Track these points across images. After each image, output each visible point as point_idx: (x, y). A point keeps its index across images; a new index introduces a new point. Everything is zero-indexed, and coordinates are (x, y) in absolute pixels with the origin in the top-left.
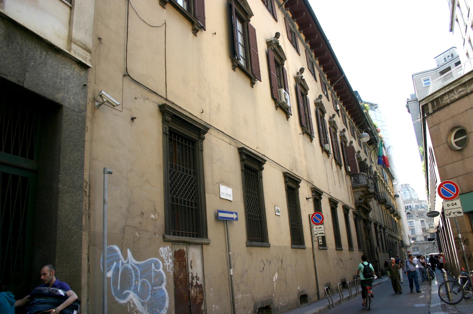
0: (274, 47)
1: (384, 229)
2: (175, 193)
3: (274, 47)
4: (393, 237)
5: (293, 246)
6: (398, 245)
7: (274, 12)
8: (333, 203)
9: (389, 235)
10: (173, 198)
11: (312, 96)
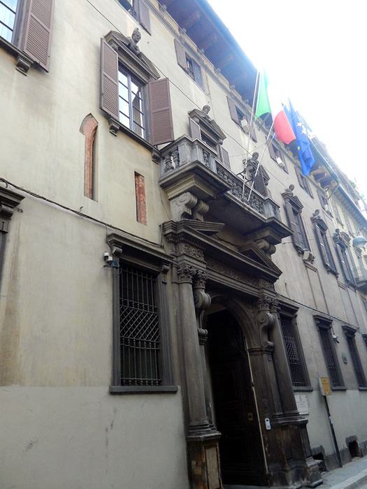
5: (119, 388)
8: (349, 333)
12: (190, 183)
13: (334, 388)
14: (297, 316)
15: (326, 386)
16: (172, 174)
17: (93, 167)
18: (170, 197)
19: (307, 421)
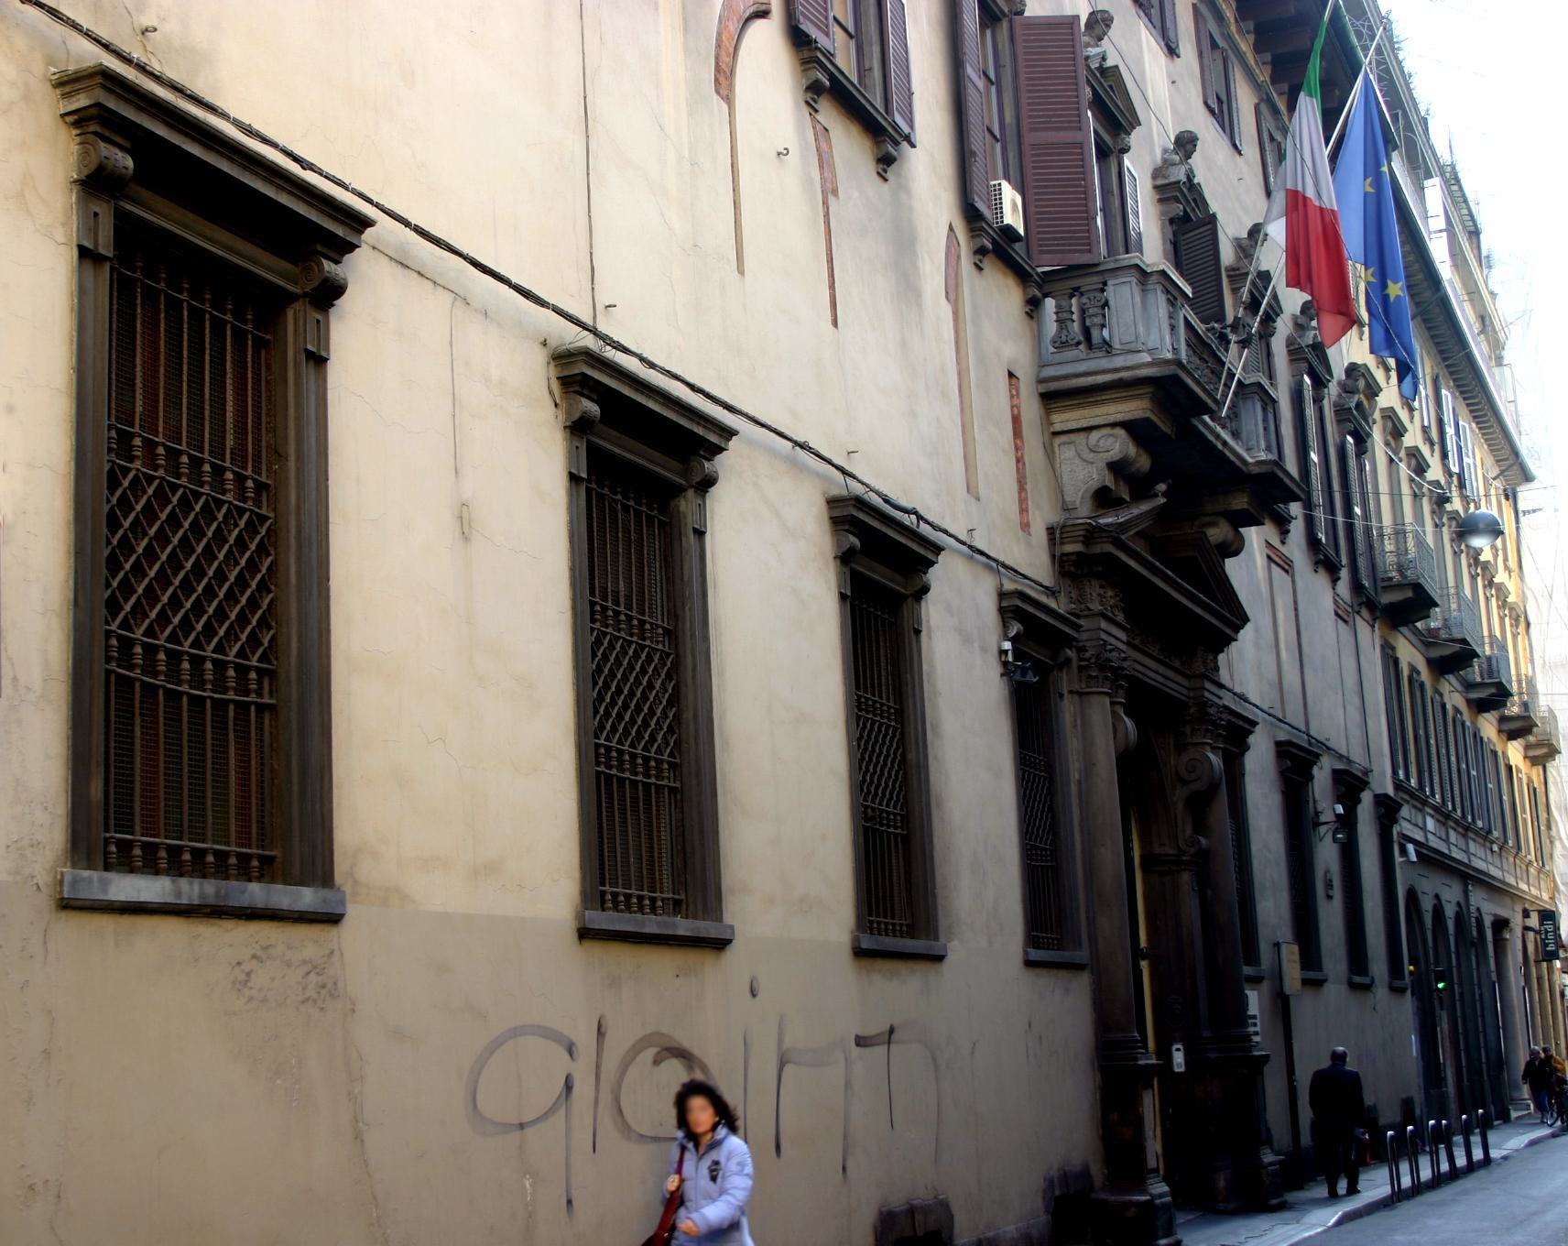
1: (1387, 811)
4: (1468, 877)
5: (1036, 954)
6: (1514, 938)
7: (1169, 24)
8: (1349, 784)
9: (1432, 860)
10: (126, 644)
12: (1134, 408)
14: (925, 589)
15: (1293, 972)
16: (1081, 366)
18: (1058, 427)
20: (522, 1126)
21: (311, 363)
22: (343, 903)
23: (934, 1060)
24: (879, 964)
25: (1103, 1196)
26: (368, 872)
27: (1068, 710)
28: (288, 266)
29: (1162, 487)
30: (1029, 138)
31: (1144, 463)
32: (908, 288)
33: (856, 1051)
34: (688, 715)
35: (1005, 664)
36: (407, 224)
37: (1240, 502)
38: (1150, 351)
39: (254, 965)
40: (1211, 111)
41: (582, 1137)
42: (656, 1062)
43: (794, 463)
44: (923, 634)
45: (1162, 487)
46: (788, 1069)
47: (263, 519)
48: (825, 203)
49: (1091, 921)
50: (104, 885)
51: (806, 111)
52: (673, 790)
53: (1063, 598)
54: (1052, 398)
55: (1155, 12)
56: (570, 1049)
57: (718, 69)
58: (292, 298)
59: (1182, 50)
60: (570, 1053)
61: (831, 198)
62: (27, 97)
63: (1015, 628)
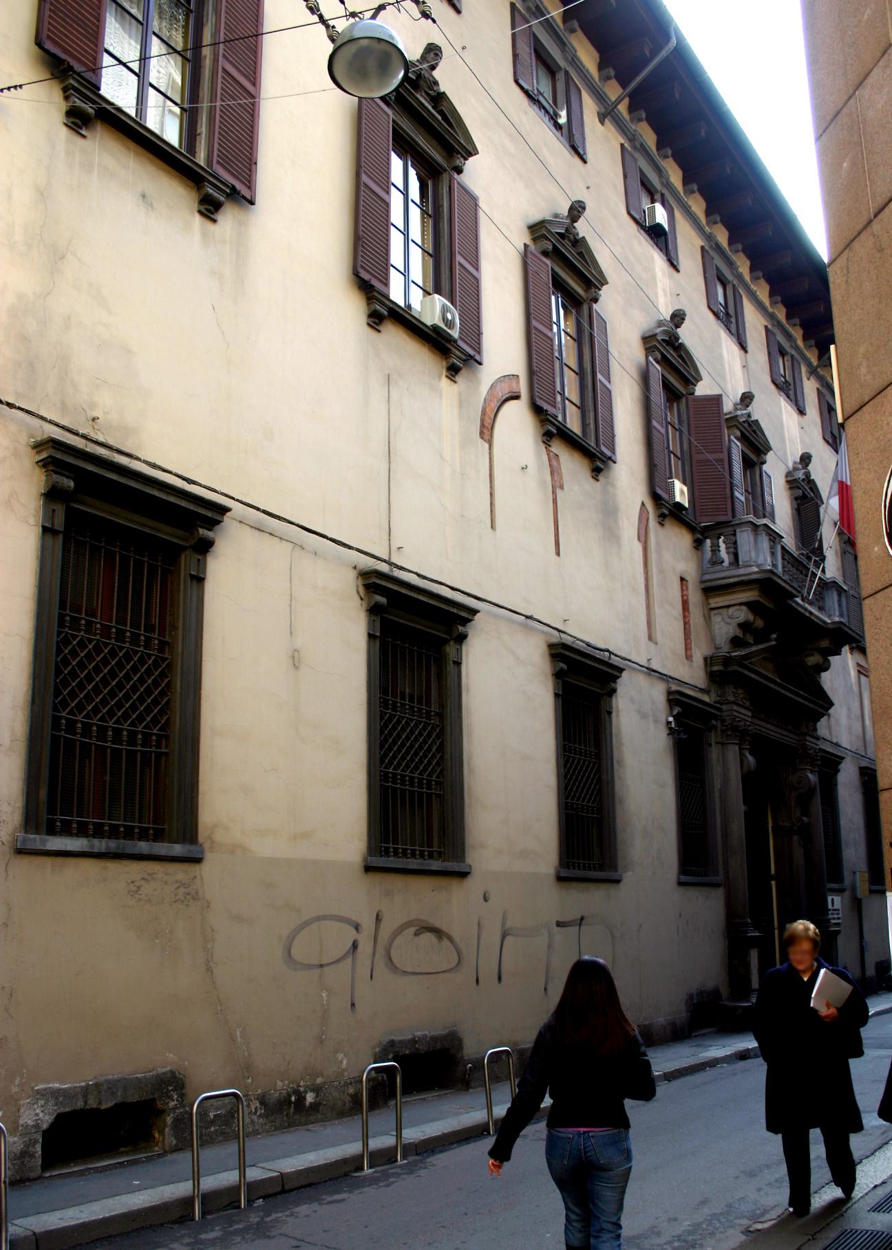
0: (668, 353)
2: (390, 763)
3: (668, 353)
5: (684, 878)
11: (624, 320)
12: (750, 595)
13: (873, 888)
14: (614, 691)
15: (862, 883)
16: (726, 573)
17: (492, 504)
18: (713, 606)
19: (839, 932)
20: (322, 966)
21: (195, 582)
22: (202, 852)
23: (612, 933)
24: (574, 884)
25: (726, 1003)
26: (219, 836)
27: (714, 753)
28: (181, 533)
29: (774, 636)
30: (696, 457)
31: (760, 623)
32: (610, 533)
33: (556, 929)
34: (447, 757)
35: (671, 729)
36: (258, 509)
37: (825, 643)
38: (758, 566)
39: (143, 883)
40: (827, 442)
41: (364, 972)
42: (416, 934)
43: (525, 626)
44: (614, 714)
45: (774, 636)
46: (508, 939)
47: (164, 659)
48: (554, 492)
49: (726, 863)
50: (44, 842)
51: (543, 447)
52: (438, 796)
53: (713, 695)
54: (709, 591)
55: (792, 393)
56: (357, 927)
57: (483, 426)
58: (185, 548)
59: (808, 410)
60: (357, 929)
61: (558, 491)
62: (16, 454)
63: (676, 710)
